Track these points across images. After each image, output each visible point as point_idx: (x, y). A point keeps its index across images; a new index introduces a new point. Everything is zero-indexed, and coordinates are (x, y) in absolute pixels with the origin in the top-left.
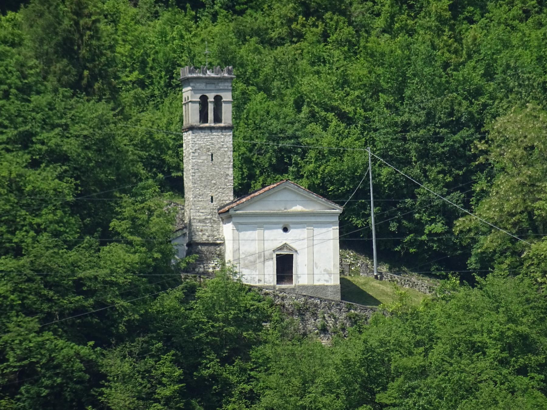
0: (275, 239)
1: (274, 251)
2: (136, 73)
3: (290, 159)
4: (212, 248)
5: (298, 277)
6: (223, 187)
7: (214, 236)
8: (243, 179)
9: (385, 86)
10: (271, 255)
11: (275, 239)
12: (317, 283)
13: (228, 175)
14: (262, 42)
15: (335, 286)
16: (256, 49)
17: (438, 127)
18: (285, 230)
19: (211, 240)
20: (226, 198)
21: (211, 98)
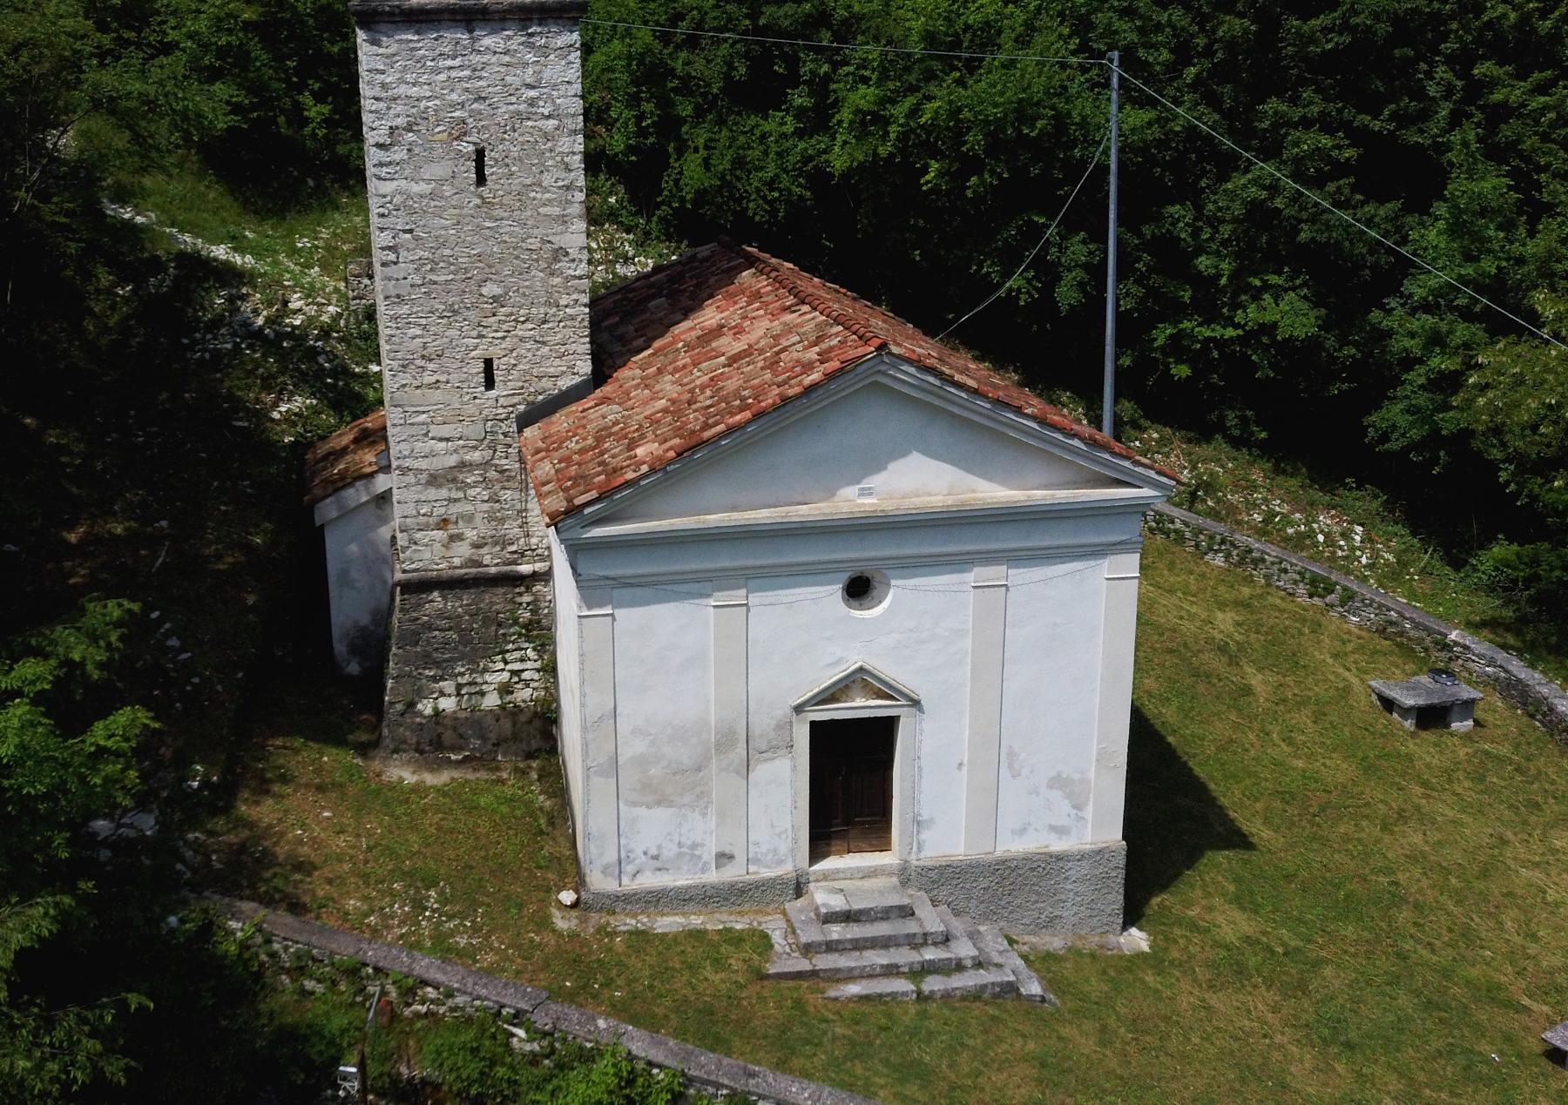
0: (804, 643)
1: (799, 709)
3: (793, 62)
4: (496, 600)
6: (538, 312)
7: (504, 542)
8: (642, 132)
10: (785, 727)
12: (1013, 845)
13: (560, 253)
18: (859, 589)
19: (492, 562)
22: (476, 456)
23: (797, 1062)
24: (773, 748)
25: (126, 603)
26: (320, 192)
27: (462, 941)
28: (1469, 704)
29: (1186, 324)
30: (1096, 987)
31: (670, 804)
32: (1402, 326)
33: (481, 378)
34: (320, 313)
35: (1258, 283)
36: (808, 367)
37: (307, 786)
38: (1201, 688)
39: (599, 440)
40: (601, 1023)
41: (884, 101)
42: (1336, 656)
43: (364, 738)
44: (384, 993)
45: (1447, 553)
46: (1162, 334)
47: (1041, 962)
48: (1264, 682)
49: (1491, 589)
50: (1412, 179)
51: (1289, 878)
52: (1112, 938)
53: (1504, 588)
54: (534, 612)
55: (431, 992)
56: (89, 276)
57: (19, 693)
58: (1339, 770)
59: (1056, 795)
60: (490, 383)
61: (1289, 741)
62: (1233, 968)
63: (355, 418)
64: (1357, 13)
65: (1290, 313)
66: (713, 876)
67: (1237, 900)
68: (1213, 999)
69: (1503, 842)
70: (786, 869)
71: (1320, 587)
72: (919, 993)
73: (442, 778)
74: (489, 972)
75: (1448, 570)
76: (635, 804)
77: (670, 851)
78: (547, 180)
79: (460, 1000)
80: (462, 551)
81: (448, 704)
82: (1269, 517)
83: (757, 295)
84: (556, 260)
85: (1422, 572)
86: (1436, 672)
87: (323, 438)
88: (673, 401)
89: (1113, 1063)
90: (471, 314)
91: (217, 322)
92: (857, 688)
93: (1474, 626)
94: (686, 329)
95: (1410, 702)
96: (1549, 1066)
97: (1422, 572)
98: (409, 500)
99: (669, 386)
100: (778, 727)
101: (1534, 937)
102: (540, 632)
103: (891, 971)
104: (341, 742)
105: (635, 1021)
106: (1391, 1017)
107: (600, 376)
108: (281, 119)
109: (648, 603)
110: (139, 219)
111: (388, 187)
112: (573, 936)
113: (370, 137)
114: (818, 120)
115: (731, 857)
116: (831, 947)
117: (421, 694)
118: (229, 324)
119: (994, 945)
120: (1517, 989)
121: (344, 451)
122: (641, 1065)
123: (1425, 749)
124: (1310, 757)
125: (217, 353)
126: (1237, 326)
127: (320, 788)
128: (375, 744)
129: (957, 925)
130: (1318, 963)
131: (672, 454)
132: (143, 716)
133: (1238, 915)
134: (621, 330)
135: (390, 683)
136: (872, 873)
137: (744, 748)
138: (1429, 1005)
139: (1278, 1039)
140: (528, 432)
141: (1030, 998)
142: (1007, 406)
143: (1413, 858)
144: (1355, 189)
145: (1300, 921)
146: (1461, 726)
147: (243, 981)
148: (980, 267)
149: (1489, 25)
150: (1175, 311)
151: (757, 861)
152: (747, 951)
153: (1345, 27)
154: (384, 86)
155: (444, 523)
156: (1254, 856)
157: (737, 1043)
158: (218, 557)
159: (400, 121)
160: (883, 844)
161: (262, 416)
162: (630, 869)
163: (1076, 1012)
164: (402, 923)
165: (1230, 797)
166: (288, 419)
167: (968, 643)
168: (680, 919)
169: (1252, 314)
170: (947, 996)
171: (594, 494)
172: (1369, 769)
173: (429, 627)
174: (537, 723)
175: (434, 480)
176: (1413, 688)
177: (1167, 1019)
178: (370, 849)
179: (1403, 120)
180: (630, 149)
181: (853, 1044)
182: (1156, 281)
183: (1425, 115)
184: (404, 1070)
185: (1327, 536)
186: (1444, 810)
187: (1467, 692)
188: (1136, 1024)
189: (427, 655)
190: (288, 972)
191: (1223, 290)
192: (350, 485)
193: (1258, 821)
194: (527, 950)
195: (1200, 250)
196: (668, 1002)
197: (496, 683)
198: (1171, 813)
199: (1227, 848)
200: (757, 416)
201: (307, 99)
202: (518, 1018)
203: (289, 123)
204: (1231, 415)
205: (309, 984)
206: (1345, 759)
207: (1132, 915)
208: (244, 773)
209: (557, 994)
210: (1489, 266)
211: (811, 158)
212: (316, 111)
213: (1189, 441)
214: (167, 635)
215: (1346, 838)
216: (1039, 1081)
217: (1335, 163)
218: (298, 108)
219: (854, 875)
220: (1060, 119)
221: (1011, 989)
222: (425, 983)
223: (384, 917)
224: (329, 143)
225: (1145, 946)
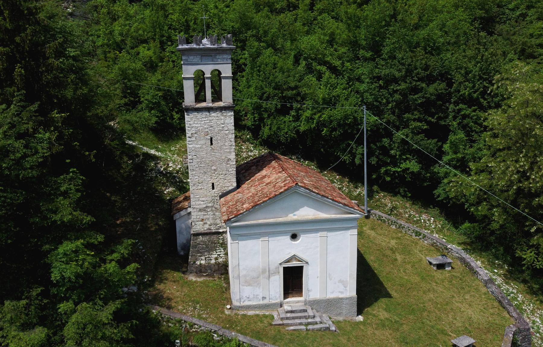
0: (281, 249)
1: (280, 264)
4: (214, 238)
5: (309, 291)
6: (224, 172)
7: (216, 224)
8: (255, 121)
9: (364, 43)
13: (229, 160)
14: (271, 12)
15: (351, 298)
16: (267, 16)
17: (414, 80)
21: (208, 75)
22: (210, 205)
23: (277, 343)
24: (275, 273)
25: (132, 241)
26: (177, 135)
27: (204, 316)
28: (449, 264)
29: (389, 168)
30: (349, 328)
31: (252, 286)
32: (440, 169)
33: (211, 187)
34: (176, 167)
36: (281, 188)
37: (171, 281)
38: (385, 259)
39: (236, 203)
40: (233, 334)
41: (312, 115)
42: (420, 251)
44: (186, 326)
46: (383, 170)
48: (401, 258)
49: (465, 234)
51: (399, 304)
52: (354, 318)
54: (223, 241)
55: (196, 326)
56: (122, 158)
57: (113, 260)
58: (416, 279)
60: (213, 188)
61: (405, 272)
62: (382, 325)
63: (184, 193)
64: (426, 94)
65: (413, 166)
66: (261, 302)
68: (376, 332)
69: (453, 297)
70: (278, 301)
71: (418, 234)
72: (307, 329)
73: (201, 279)
74: (210, 323)
76: (243, 286)
77: (251, 296)
78: (226, 144)
79: (203, 328)
80: (207, 226)
81: (203, 262)
82: (410, 215)
83: (274, 168)
84: (228, 161)
85: (448, 230)
87: (176, 198)
88: (253, 194)
90: (209, 173)
91: (152, 170)
92: (294, 259)
93: (459, 244)
94: (258, 175)
95: (435, 263)
97: (448, 230)
98: (195, 215)
99: (253, 190)
100: (276, 268)
101: (456, 319)
102: (224, 245)
103: (301, 324)
104: (179, 271)
105: (242, 334)
106: (418, 337)
107: (238, 186)
108: (168, 118)
109: (246, 240)
110: (134, 144)
111: (191, 146)
112: (229, 315)
113: (187, 135)
114: (297, 118)
115: (265, 298)
116: (287, 318)
117: (197, 260)
119: (325, 317)
121: (181, 202)
122: (241, 343)
123: (439, 274)
124: (410, 276)
125: (152, 178)
126: (401, 168)
127: (174, 282)
128: (187, 271)
129: (317, 314)
130: (402, 324)
132: (137, 265)
133: (385, 313)
134: (245, 174)
135: (190, 257)
136: (298, 302)
137: (269, 273)
139: (390, 341)
140: (222, 199)
141: (332, 331)
142: (325, 197)
145: (400, 315)
146: (448, 269)
147: (156, 323)
148: (337, 153)
149: (461, 95)
150: (386, 164)
151: (271, 299)
152: (268, 319)
153: (423, 97)
154: (190, 124)
155: (202, 220)
156: (392, 299)
157: (264, 339)
158: (152, 227)
159: (194, 132)
160: (301, 296)
163: (343, 334)
164: (191, 312)
165: (388, 285)
166: (169, 193)
167: (319, 249)
168: (254, 312)
169: (403, 166)
170: (313, 330)
171: (234, 216)
172: (423, 279)
173: (199, 244)
174: (224, 267)
175: (200, 210)
178: (184, 295)
179: (440, 118)
180: (253, 125)
181: (290, 340)
182: (381, 157)
183: (447, 117)
184: (190, 344)
186: (440, 289)
187: (449, 260)
188: (357, 337)
189: (198, 251)
190: (165, 322)
191: (398, 159)
192: (182, 210)
193: (394, 291)
194: (219, 319)
195: (392, 149)
196: (250, 330)
197: (214, 257)
199: (385, 297)
200: (270, 199)
201: (174, 113)
202: (215, 332)
203: (170, 119)
204: (401, 190)
205: (170, 324)
206: (417, 276)
208: (157, 278)
209: (225, 328)
210: (460, 156)
211: (296, 127)
212: (176, 116)
214: (140, 246)
215: (415, 295)
217: (422, 130)
218: (172, 115)
219: (294, 302)
220: (355, 119)
221: (328, 329)
222: (195, 324)
223: (187, 310)
224: (180, 124)
225: (362, 320)
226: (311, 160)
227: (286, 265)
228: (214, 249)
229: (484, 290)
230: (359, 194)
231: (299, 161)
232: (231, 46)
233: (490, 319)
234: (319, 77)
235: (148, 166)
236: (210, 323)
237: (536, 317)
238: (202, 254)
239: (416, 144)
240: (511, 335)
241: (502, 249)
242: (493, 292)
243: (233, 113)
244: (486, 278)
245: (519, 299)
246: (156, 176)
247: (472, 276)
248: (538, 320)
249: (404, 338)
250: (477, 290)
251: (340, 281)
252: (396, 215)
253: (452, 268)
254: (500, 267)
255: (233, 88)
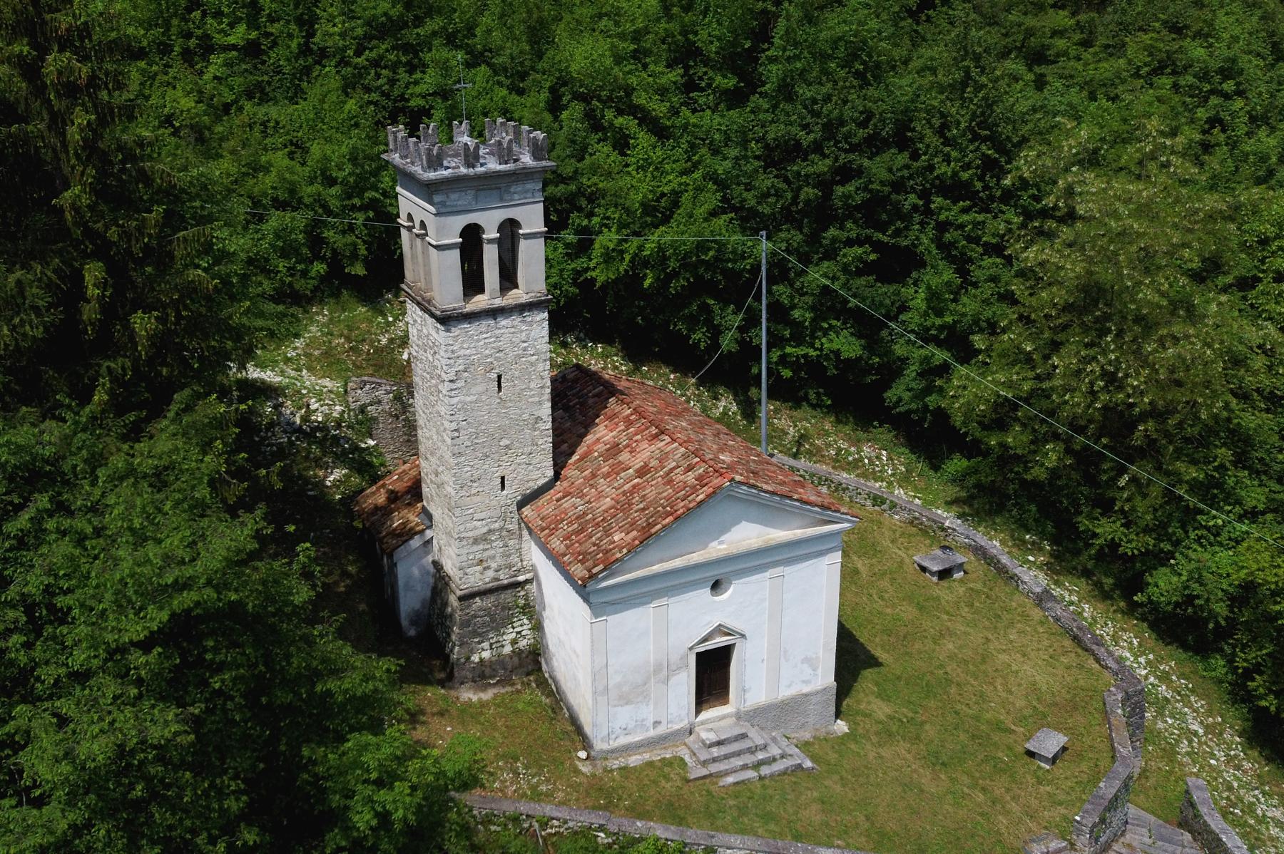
0: (692, 619)
1: (691, 649)
2: (241, 28)
4: (507, 597)
11: (692, 619)
12: (786, 693)
13: (539, 419)
20: (537, 474)
21: (491, 233)
23: (719, 823)
27: (543, 788)
28: (960, 567)
30: (833, 757)
35: (826, 325)
40: (639, 824)
41: (620, 242)
43: (443, 675)
45: (931, 463)
47: (805, 746)
50: (897, 265)
51: (899, 678)
53: (959, 480)
59: (805, 666)
60: (503, 487)
61: (881, 598)
62: (886, 735)
64: (872, 183)
65: (845, 344)
66: (652, 733)
67: (879, 696)
68: (883, 752)
69: (988, 640)
70: (684, 724)
73: (487, 696)
75: (932, 473)
78: (532, 385)
79: (571, 824)
86: (944, 548)
89: (850, 794)
90: (496, 456)
91: (272, 425)
93: (949, 504)
95: (935, 569)
96: (1029, 760)
101: (1011, 692)
102: (532, 611)
103: (745, 767)
104: (430, 683)
109: (621, 611)
112: (594, 775)
116: (714, 760)
117: (472, 652)
118: (279, 424)
120: (1008, 721)
123: (944, 592)
124: (894, 606)
130: (923, 723)
131: (637, 542)
137: (664, 671)
138: (973, 737)
141: (808, 769)
143: (952, 657)
144: (876, 281)
145: (909, 702)
146: (958, 575)
148: (675, 325)
149: (938, 177)
153: (866, 189)
154: (453, 352)
159: (461, 368)
161: (321, 484)
162: (613, 736)
166: (336, 484)
168: (638, 757)
170: (772, 775)
171: (601, 567)
172: (921, 608)
173: (475, 616)
175: (476, 541)
176: (934, 559)
177: (866, 767)
179: (897, 233)
185: (870, 459)
189: (475, 631)
192: (411, 538)
193: (879, 649)
195: (793, 307)
198: (852, 658)
202: (601, 828)
207: (838, 715)
213: (791, 408)
216: (823, 811)
221: (799, 766)
226: (608, 341)
227: (701, 649)
228: (508, 621)
229: (1037, 614)
230: (725, 413)
231: (585, 347)
232: (544, 163)
233: (1068, 679)
234: (622, 143)
235: (261, 416)
236: (561, 804)
237: (1123, 647)
238: (483, 637)
239: (854, 296)
240: (1119, 711)
241: (1033, 508)
242: (1057, 619)
243: (546, 314)
244: (1038, 590)
245: (1085, 615)
246: (291, 443)
247: (1006, 584)
248: (1128, 655)
249: (937, 755)
250: (1025, 617)
251: (807, 660)
252: (809, 452)
253: (965, 572)
254: (1036, 548)
255: (547, 260)
